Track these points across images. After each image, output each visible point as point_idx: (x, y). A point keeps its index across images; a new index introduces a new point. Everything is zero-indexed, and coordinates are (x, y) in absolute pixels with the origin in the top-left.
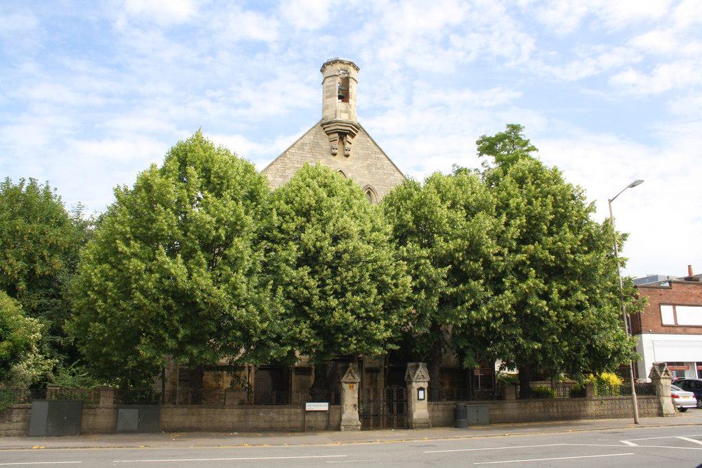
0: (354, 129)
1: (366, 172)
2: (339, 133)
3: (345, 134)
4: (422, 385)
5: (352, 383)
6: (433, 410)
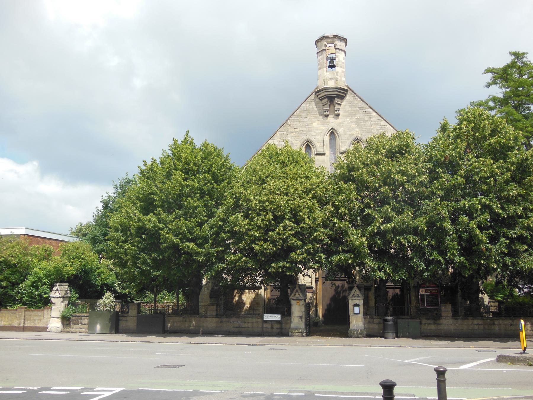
0: (338, 91)
1: (355, 126)
2: (328, 98)
3: (334, 98)
4: (357, 302)
5: (298, 300)
6: (369, 322)
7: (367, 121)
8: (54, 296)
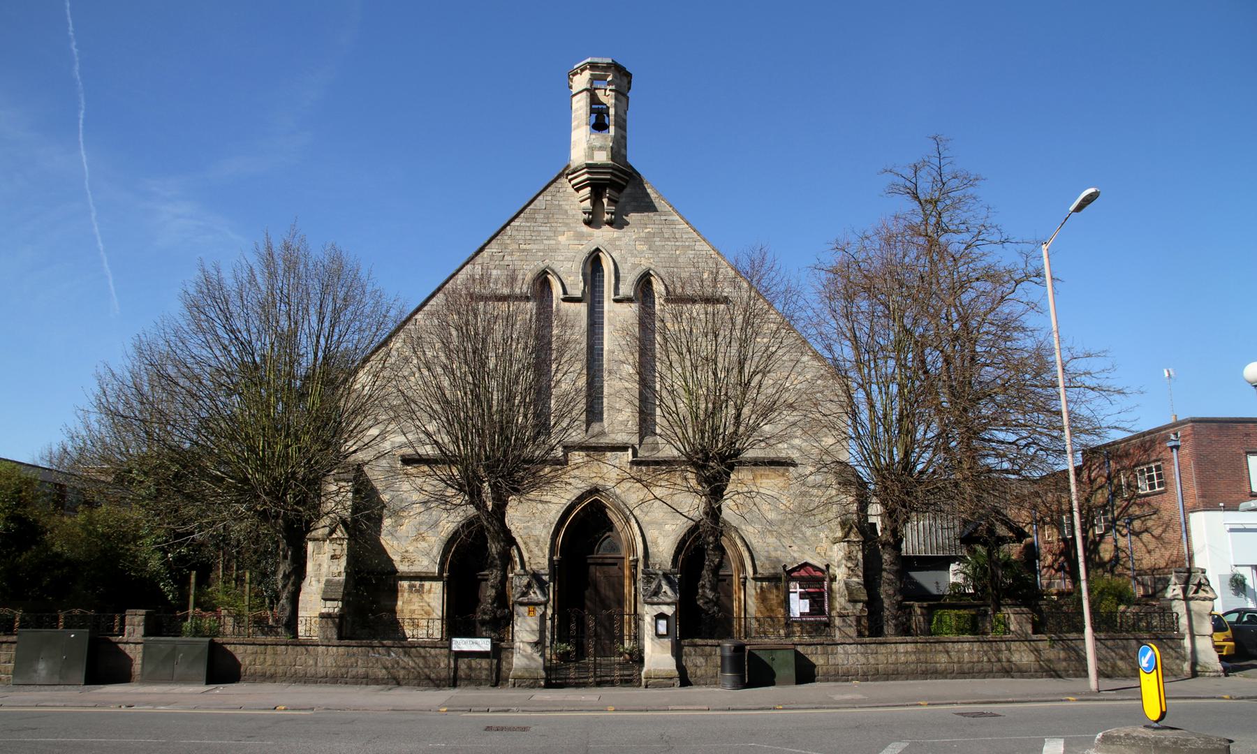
7: (668, 239)
8: (525, 599)
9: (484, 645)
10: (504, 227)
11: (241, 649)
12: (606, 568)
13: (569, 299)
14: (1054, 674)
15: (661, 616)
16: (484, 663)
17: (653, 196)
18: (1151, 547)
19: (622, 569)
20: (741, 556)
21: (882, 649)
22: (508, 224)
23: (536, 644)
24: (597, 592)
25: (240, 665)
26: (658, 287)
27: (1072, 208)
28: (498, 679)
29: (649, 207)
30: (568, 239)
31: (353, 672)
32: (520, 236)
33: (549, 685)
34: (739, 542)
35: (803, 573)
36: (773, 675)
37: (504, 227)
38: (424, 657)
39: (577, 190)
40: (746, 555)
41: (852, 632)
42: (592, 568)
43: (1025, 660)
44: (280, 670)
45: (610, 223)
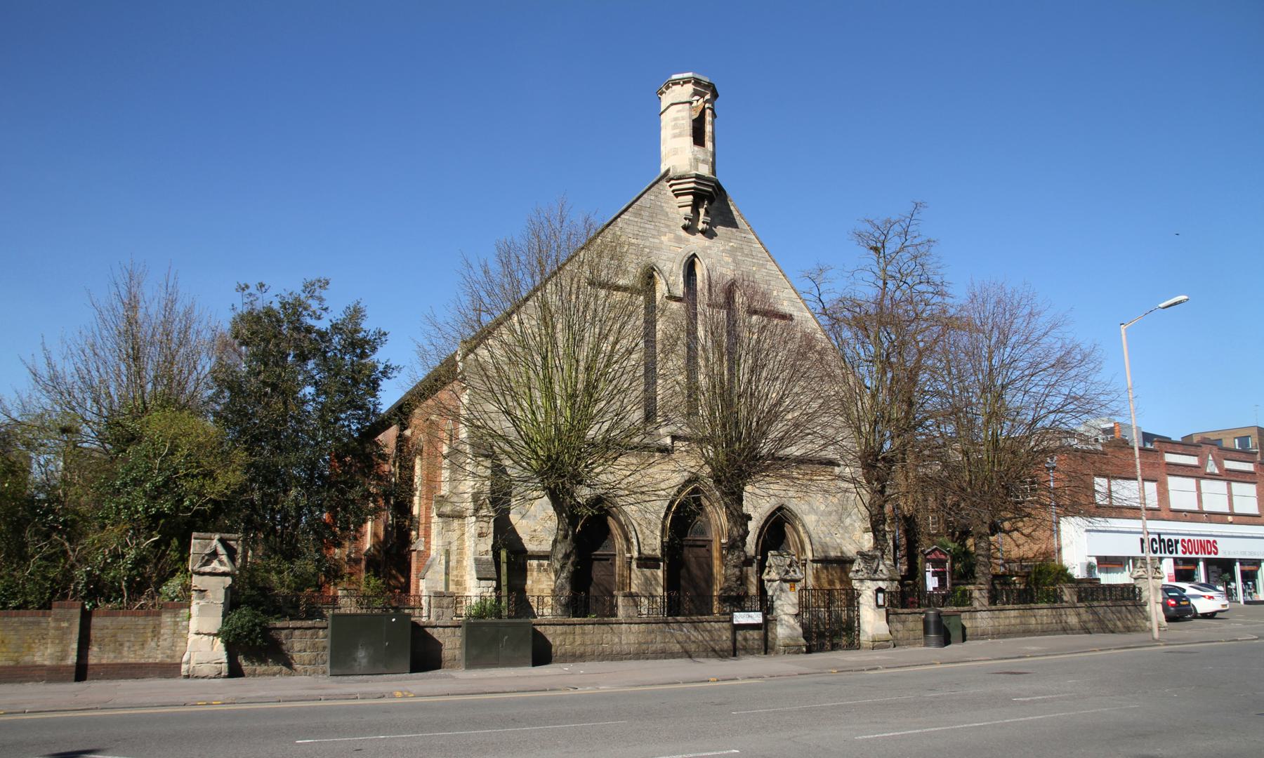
9: (757, 618)
10: (616, 218)
11: (551, 629)
12: (696, 550)
13: (672, 298)
14: (1088, 631)
15: (879, 590)
16: (755, 634)
17: (735, 213)
18: (1020, 542)
19: (709, 551)
20: (802, 542)
21: (1002, 614)
22: (619, 216)
23: (796, 615)
24: (689, 571)
25: (550, 646)
26: (739, 299)
27: (1161, 305)
28: (767, 647)
29: (731, 223)
30: (670, 240)
31: (653, 648)
32: (629, 229)
33: (810, 650)
34: (801, 529)
35: (933, 556)
36: (440, 661)
37: (616, 218)
38: (709, 632)
39: (677, 196)
40: (807, 541)
41: (985, 601)
42: (686, 550)
43: (632, 638)
44: (589, 649)
45: (703, 232)
